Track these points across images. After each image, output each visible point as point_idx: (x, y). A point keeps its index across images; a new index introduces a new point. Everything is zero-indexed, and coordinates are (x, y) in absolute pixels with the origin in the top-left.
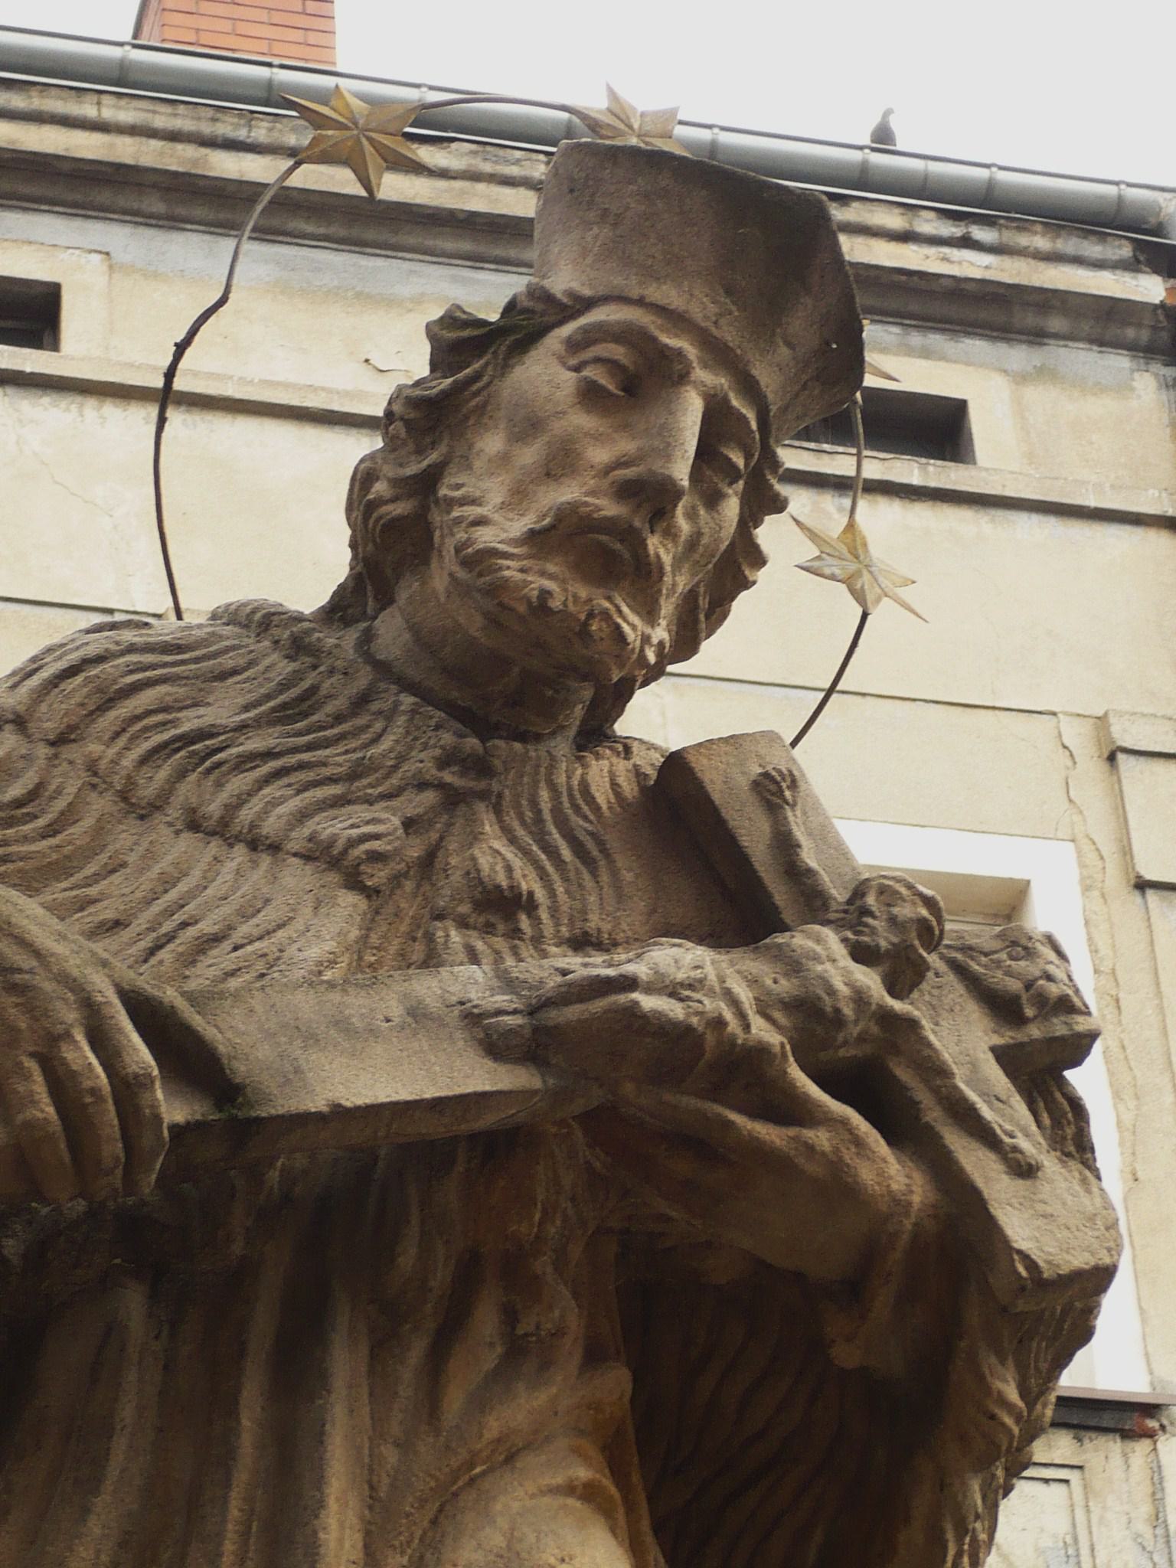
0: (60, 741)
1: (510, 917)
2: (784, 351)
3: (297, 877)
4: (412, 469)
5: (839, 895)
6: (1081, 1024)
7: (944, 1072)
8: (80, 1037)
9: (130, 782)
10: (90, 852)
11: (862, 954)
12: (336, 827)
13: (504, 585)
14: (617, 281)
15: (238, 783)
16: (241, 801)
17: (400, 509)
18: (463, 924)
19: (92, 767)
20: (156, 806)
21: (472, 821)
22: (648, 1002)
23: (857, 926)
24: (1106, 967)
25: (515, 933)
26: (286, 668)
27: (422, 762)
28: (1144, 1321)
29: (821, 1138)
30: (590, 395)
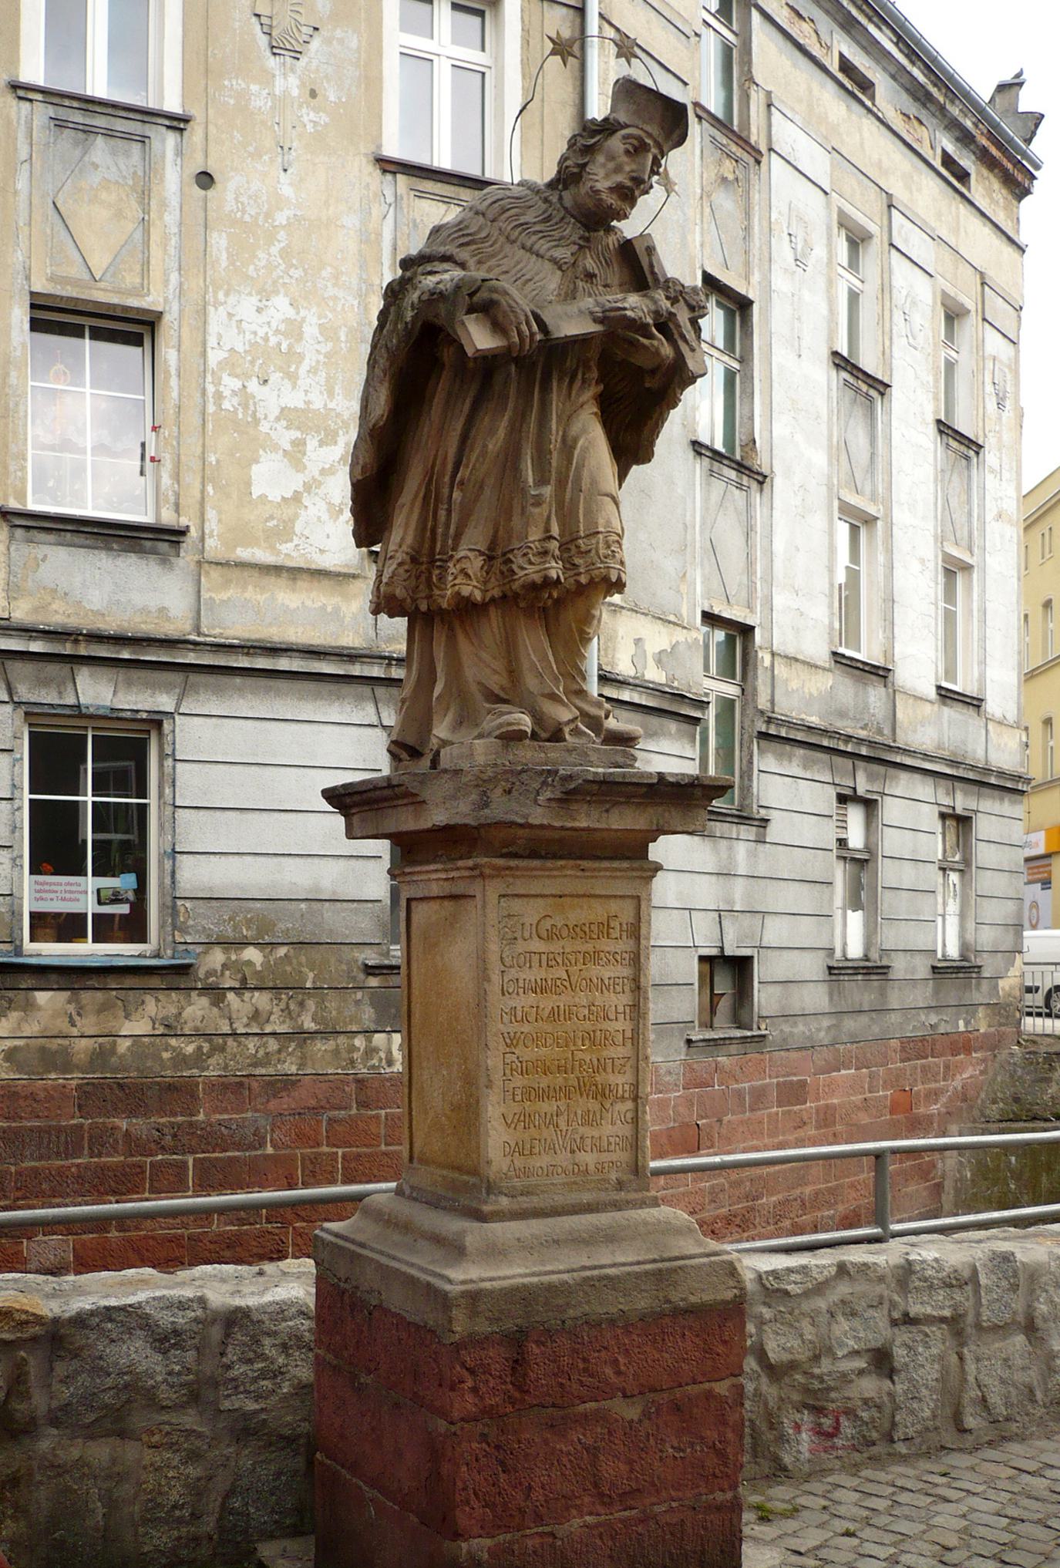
0: (493, 221)
3: (548, 265)
4: (581, 162)
5: (662, 280)
7: (680, 326)
10: (500, 251)
11: (668, 298)
13: (601, 199)
15: (534, 238)
16: (535, 242)
17: (575, 170)
20: (514, 242)
21: (585, 253)
22: (629, 313)
23: (667, 291)
24: (526, 28)
25: (592, 283)
26: (544, 206)
27: (575, 237)
28: (522, 159)
29: (655, 343)
30: (627, 152)
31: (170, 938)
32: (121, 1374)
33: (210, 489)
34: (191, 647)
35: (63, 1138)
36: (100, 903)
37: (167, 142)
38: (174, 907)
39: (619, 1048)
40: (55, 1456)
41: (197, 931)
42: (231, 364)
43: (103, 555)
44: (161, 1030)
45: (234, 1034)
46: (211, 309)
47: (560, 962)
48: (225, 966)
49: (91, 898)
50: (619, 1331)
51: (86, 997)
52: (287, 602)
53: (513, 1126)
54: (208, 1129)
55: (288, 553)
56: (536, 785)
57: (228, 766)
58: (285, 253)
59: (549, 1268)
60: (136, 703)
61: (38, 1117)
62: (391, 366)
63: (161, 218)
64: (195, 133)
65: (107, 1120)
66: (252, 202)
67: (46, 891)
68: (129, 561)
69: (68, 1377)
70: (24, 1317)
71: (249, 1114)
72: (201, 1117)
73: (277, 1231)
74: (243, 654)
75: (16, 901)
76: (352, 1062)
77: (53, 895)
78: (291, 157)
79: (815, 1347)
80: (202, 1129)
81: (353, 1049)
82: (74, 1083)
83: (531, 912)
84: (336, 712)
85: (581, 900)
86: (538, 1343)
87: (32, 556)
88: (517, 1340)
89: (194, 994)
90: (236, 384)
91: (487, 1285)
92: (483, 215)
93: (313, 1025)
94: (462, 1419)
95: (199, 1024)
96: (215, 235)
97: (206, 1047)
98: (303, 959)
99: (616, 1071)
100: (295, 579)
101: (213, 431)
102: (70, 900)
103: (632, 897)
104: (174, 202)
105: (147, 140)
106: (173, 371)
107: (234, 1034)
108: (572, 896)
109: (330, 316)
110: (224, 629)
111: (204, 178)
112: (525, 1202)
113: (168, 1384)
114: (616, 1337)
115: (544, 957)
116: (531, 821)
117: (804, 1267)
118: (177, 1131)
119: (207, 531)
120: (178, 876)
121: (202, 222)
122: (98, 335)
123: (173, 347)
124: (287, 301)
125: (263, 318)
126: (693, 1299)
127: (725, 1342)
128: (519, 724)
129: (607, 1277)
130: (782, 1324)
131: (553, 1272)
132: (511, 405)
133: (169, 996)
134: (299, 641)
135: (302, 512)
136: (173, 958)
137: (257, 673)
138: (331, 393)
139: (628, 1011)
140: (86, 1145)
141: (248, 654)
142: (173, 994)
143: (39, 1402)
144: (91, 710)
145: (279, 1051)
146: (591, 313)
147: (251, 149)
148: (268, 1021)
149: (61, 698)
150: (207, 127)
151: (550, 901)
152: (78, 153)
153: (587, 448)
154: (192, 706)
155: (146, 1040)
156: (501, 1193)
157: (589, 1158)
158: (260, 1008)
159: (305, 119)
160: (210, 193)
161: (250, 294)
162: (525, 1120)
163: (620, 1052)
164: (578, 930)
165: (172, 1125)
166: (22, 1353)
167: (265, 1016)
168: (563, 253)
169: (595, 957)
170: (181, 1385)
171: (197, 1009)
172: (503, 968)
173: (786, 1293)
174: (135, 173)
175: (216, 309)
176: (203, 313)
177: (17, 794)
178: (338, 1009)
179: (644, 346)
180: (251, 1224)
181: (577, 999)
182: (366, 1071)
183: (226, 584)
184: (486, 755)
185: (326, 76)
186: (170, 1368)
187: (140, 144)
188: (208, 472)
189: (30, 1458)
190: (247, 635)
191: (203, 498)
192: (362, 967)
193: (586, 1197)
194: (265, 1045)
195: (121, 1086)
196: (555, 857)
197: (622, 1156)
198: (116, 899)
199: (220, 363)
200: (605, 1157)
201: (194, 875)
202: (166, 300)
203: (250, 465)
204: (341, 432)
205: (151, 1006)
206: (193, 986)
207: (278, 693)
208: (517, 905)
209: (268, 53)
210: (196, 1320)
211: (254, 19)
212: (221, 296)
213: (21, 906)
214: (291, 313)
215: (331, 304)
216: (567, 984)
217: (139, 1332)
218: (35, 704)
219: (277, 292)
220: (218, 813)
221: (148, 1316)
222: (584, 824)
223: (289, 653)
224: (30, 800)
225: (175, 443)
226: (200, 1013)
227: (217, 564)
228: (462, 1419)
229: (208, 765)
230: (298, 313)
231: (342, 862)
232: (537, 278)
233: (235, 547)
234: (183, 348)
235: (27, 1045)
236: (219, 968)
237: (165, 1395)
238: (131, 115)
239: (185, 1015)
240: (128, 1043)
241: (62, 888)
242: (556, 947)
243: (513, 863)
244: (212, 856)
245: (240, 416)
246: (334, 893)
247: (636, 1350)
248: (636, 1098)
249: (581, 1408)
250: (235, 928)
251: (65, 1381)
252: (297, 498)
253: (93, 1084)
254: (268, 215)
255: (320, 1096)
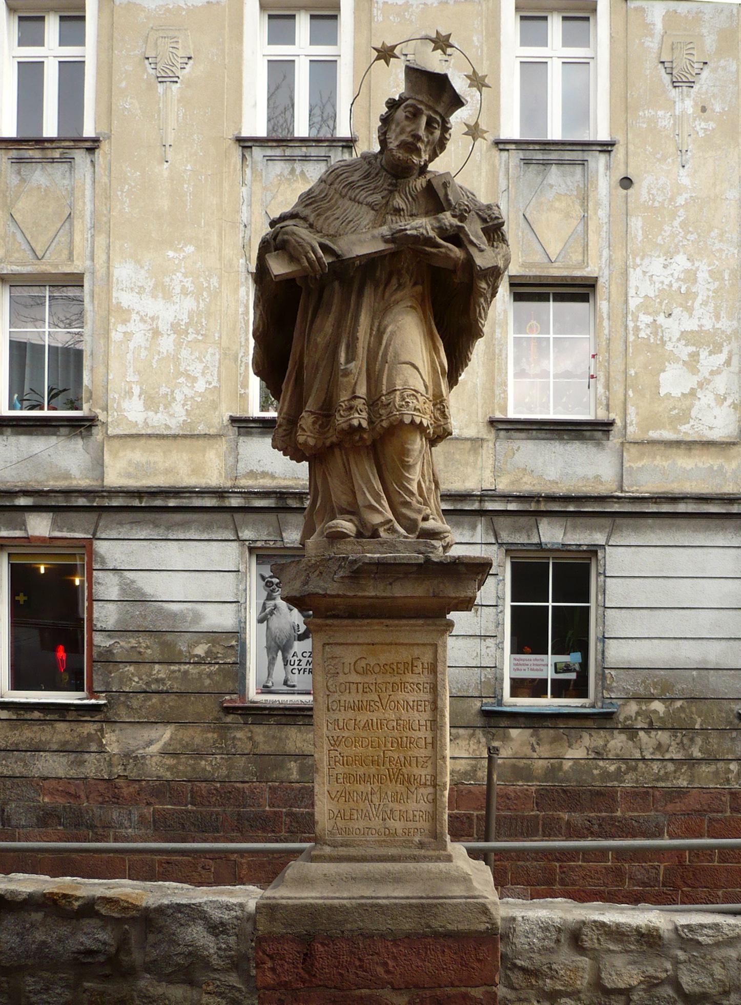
0: (331, 184)
1: (399, 212)
2: (442, 104)
3: (365, 208)
6: (500, 221)
8: (311, 252)
9: (341, 192)
11: (454, 216)
12: (370, 199)
14: (413, 95)
15: (357, 191)
16: (357, 195)
18: (391, 214)
19: (335, 190)
21: (394, 195)
22: (409, 232)
29: (443, 250)
30: (407, 117)
31: (601, 695)
32: (187, 946)
33: (630, 393)
34: (615, 500)
35: (525, 824)
36: (556, 672)
37: (599, 162)
38: (603, 674)
39: (421, 750)
40: (148, 990)
41: (619, 690)
42: (645, 307)
43: (557, 443)
44: (593, 756)
45: (643, 759)
46: (631, 270)
47: (374, 690)
48: (638, 713)
49: (551, 669)
50: (389, 944)
51: (543, 733)
52: (684, 465)
53: (336, 799)
54: (623, 822)
55: (687, 431)
56: (335, 568)
57: (642, 579)
58: (683, 224)
59: (337, 895)
60: (579, 540)
61: (510, 809)
62: (262, 295)
63: (596, 213)
64: (619, 152)
65: (555, 813)
66: (659, 192)
67: (520, 665)
68: (574, 446)
69: (155, 944)
70: (126, 904)
71: (653, 813)
72: (619, 814)
73: (670, 892)
74: (652, 503)
75: (498, 671)
76: (728, 780)
77: (525, 667)
78: (687, 157)
79: (725, 985)
80: (619, 821)
81: (729, 771)
82: (534, 788)
83: (349, 656)
84: (720, 539)
85: (390, 647)
86: (323, 944)
87: (510, 448)
88: (307, 942)
89: (616, 732)
90: (648, 319)
91: (284, 902)
92: (325, 182)
93: (700, 754)
94: (264, 988)
95: (619, 752)
96: (633, 219)
97: (624, 767)
98: (694, 709)
99: (420, 767)
100: (690, 449)
101: (632, 353)
102: (537, 670)
103: (431, 645)
104: (605, 201)
105: (586, 163)
106: (605, 316)
107: (644, 759)
108: (382, 644)
109: (717, 263)
110: (639, 486)
111: (626, 181)
112: (343, 851)
113: (218, 955)
114: (387, 947)
115: (360, 686)
116: (328, 592)
117: (717, 925)
118: (601, 822)
119: (628, 422)
120: (606, 654)
121: (625, 213)
122: (560, 298)
123: (606, 299)
124: (685, 257)
125: (669, 271)
126: (450, 927)
127: (479, 960)
128: (336, 527)
129: (378, 905)
130: (696, 965)
131: (338, 898)
132: (334, 308)
133: (598, 733)
134: (693, 491)
135: (697, 402)
136: (602, 708)
137: (663, 515)
138: (718, 317)
139: (428, 724)
140: (541, 829)
141: (655, 503)
142: (602, 732)
143: (137, 957)
144: (549, 546)
145: (675, 772)
146: (383, 237)
147: (659, 156)
148: (667, 751)
149: (529, 539)
150: (627, 147)
151: (364, 647)
152: (539, 179)
153: (395, 332)
154: (617, 540)
155: (582, 761)
156: (325, 843)
157: (397, 825)
158: (662, 742)
159: (698, 128)
160: (630, 191)
161: (659, 256)
162: (346, 795)
163: (423, 753)
164: (387, 667)
165: (599, 818)
166: (126, 927)
167: (665, 747)
168: (377, 198)
169: (402, 686)
170: (226, 957)
171: (618, 742)
172: (328, 693)
173: (698, 942)
174: (578, 186)
175: (635, 269)
176: (625, 274)
177: (500, 602)
178: (718, 744)
179: (434, 254)
180: (651, 886)
181: (387, 715)
182: (738, 787)
183: (642, 456)
184: (316, 549)
185: (714, 95)
186: (219, 946)
187: (581, 167)
188: (629, 381)
189: (133, 990)
190: (655, 490)
191: (625, 400)
192: (737, 715)
193: (392, 851)
194: (665, 767)
195: (565, 791)
196: (368, 617)
197: (425, 825)
198: (567, 669)
199: (637, 306)
200: (410, 825)
201: (617, 653)
202: (600, 268)
203: (659, 374)
204: (725, 344)
205: (586, 740)
206: (615, 726)
207: (679, 528)
208: (338, 651)
209: (671, 87)
210: (237, 918)
211: (660, 66)
212: (638, 260)
213: (502, 674)
214: (688, 265)
215: (718, 255)
216: (379, 705)
217: (200, 921)
218: (512, 544)
219: (678, 252)
220: (635, 611)
221: (205, 912)
222: (373, 594)
223: (685, 501)
224: (512, 607)
225: (606, 364)
226: (620, 745)
227: (635, 443)
228: (264, 988)
229: (628, 580)
230: (693, 265)
231: (723, 643)
232: (355, 219)
233: (648, 432)
234: (612, 299)
235: (504, 763)
236: (634, 715)
237: (215, 961)
238: (574, 148)
239: (609, 745)
240: (570, 763)
241: (532, 662)
242: (370, 679)
243: (329, 622)
244: (630, 640)
245: (652, 341)
246: (717, 664)
247: (403, 958)
248: (435, 786)
249: (358, 992)
250: (645, 688)
251: (154, 946)
252: (693, 393)
253: (546, 789)
254: (672, 199)
255: (703, 803)
